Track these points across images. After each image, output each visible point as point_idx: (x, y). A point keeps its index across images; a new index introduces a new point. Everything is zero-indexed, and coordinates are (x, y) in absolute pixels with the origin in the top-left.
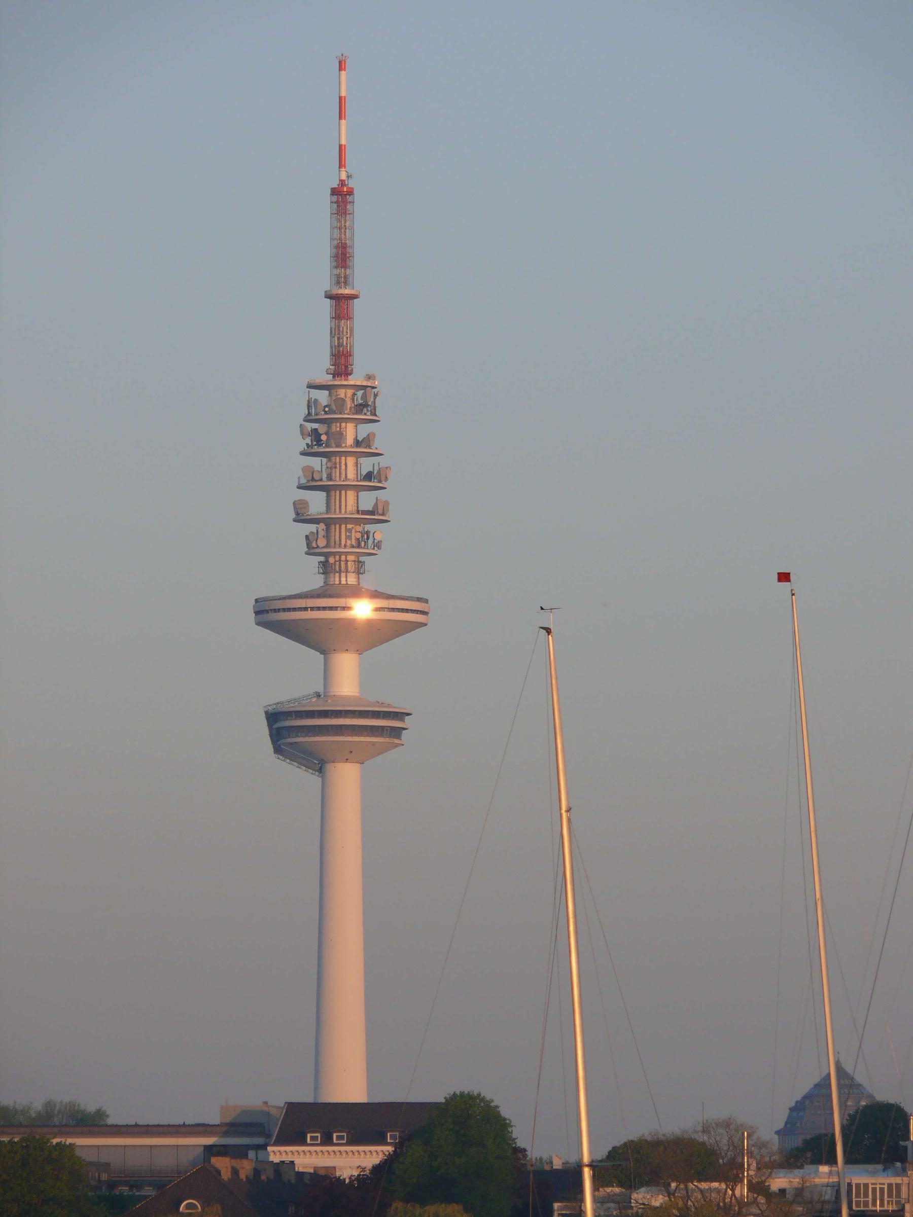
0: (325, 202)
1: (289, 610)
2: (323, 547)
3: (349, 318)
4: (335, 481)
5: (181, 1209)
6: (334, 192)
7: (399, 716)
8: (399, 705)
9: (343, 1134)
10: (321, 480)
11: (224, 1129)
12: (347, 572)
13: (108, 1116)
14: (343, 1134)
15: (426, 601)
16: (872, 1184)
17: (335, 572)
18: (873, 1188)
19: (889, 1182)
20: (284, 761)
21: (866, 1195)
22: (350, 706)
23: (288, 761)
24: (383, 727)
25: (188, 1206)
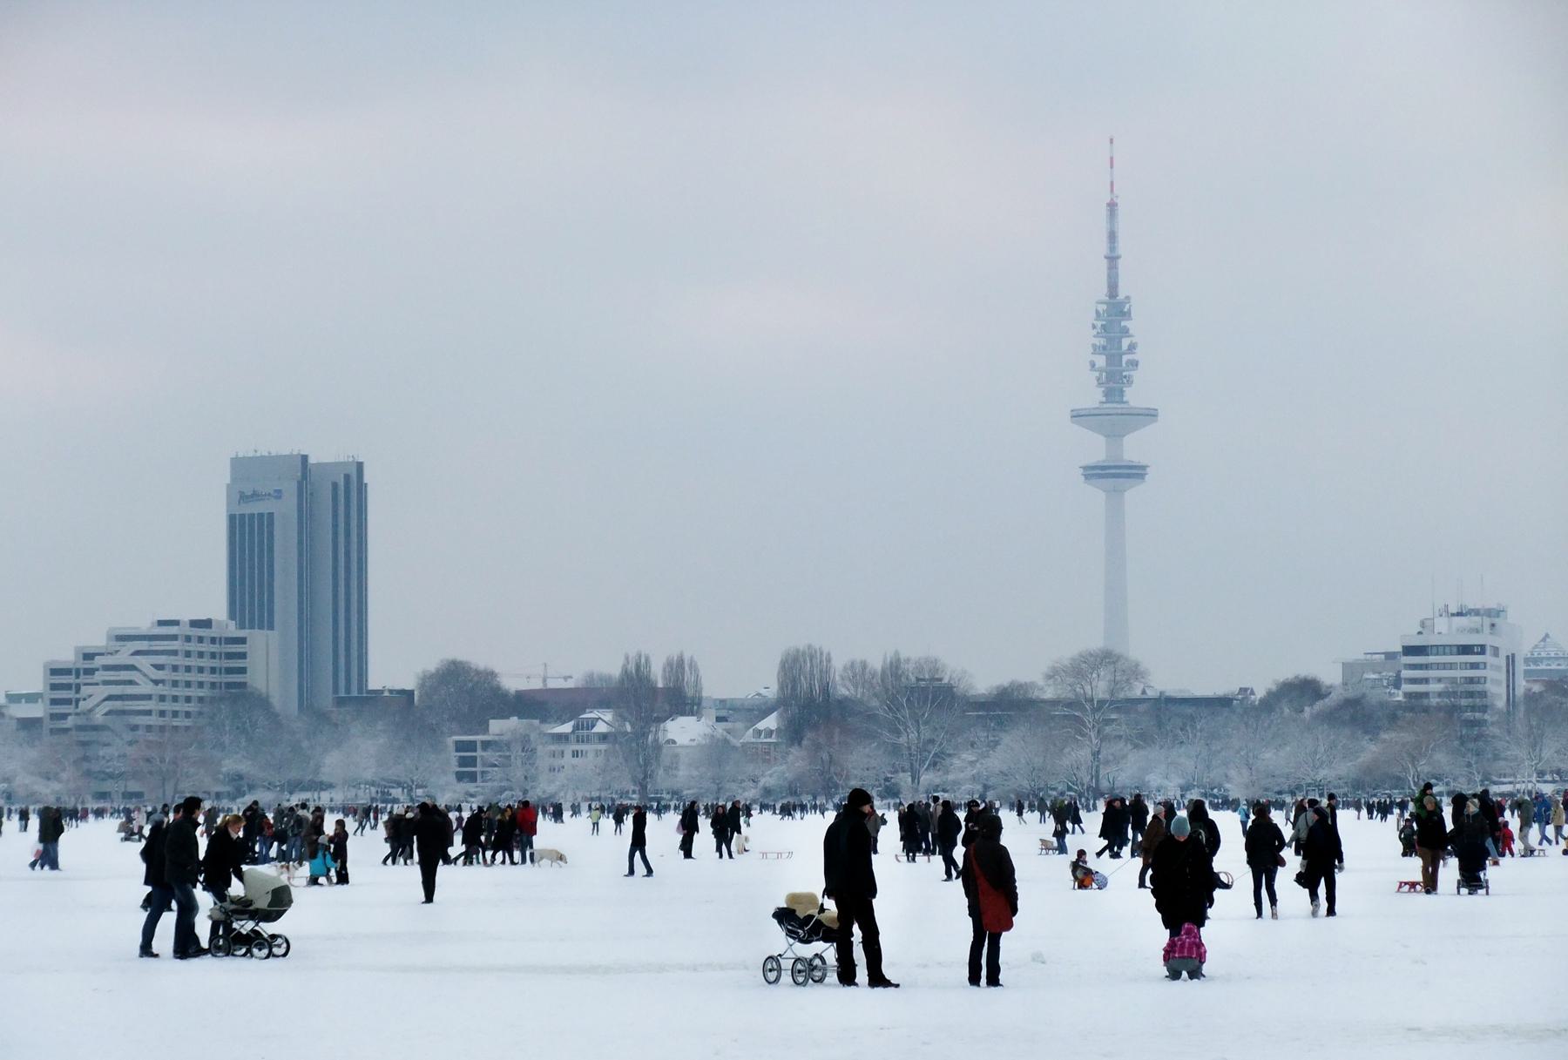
0: (1103, 211)
3: (1117, 268)
7: (1144, 468)
8: (1144, 463)
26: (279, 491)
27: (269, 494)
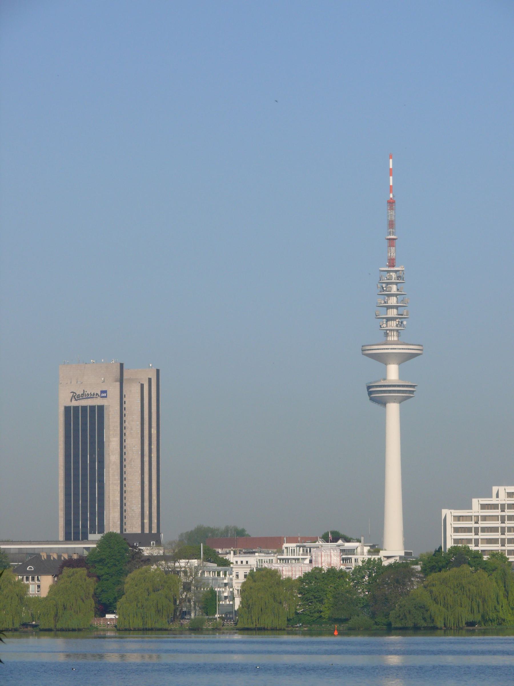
1: (371, 350)
2: (385, 327)
4: (389, 304)
5: (27, 569)
6: (389, 202)
9: (152, 543)
10: (381, 303)
11: (97, 542)
12: (394, 336)
13: (246, 531)
14: (152, 543)
15: (422, 346)
16: (264, 559)
17: (390, 336)
18: (264, 561)
19: (269, 559)
20: (373, 403)
21: (262, 563)
22: (394, 383)
23: (374, 402)
24: (406, 391)
25: (30, 568)
26: (105, 392)
27: (97, 394)
